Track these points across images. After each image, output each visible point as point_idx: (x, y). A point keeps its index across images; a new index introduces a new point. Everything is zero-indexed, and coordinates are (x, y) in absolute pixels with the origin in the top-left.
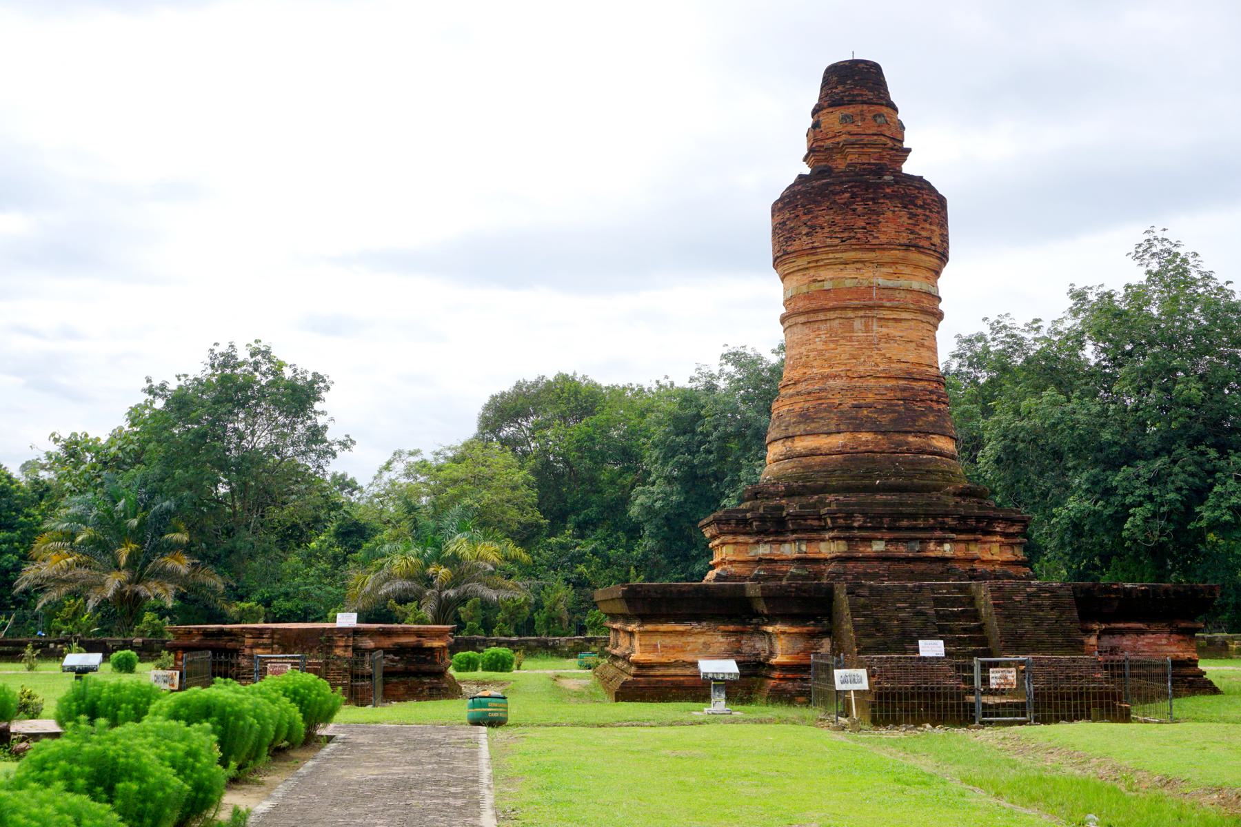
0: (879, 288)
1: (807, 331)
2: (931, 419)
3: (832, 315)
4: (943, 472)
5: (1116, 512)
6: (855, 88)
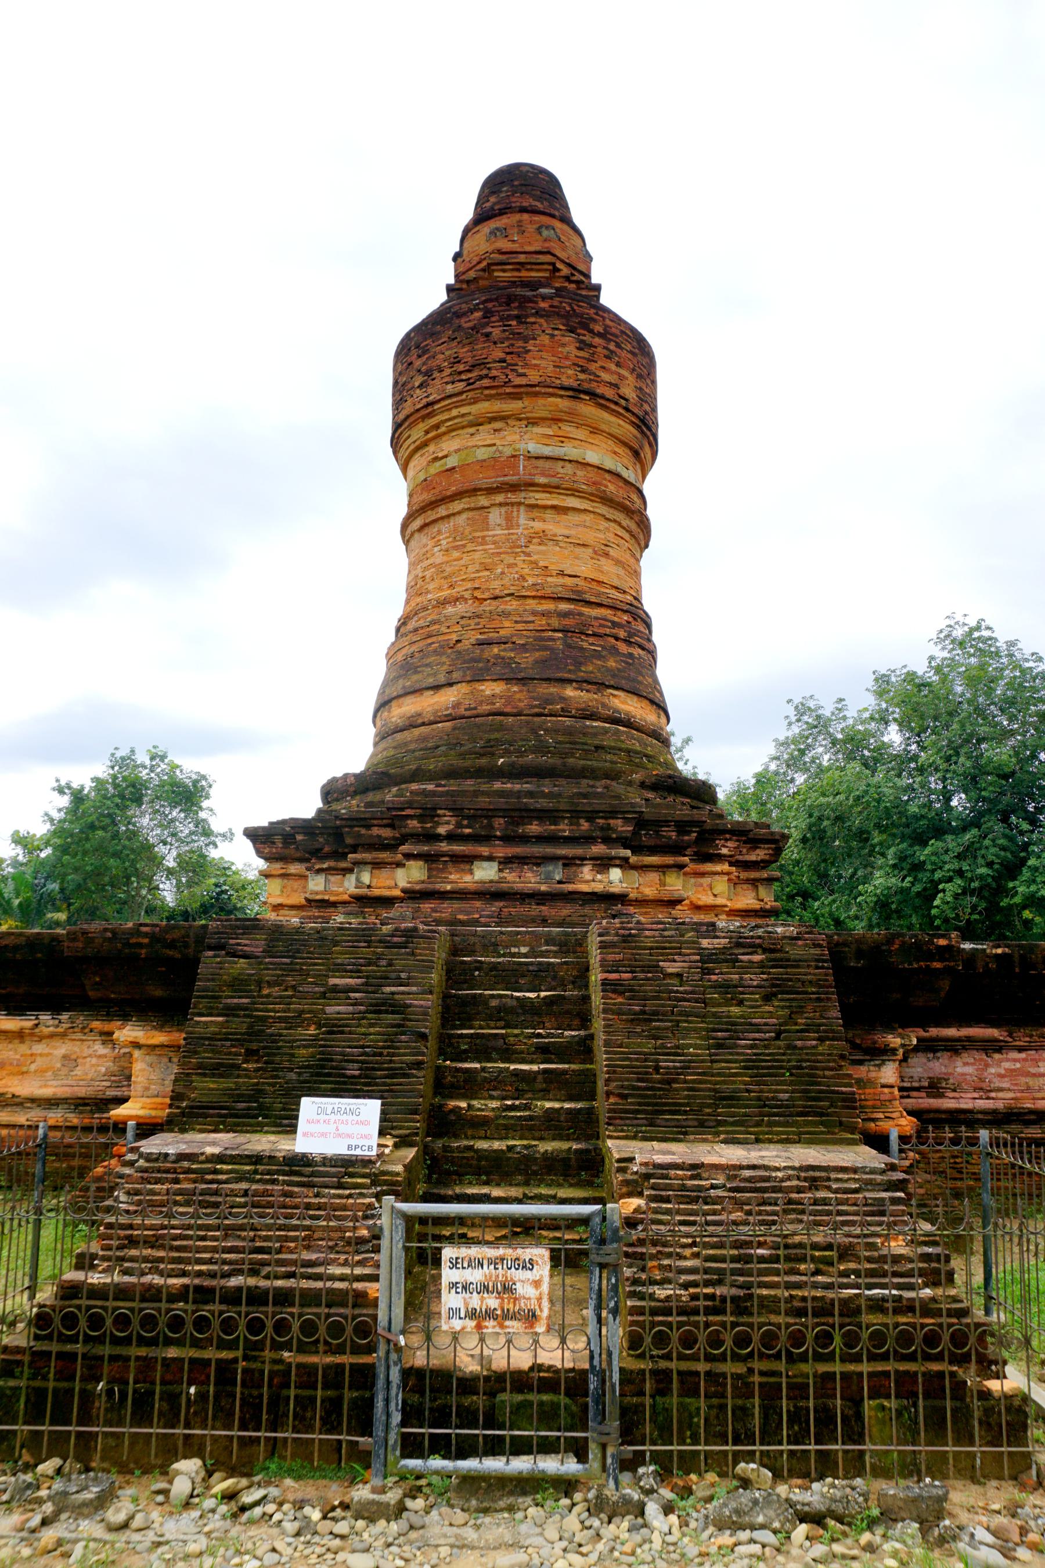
0: (530, 457)
1: (424, 540)
2: (612, 663)
3: (457, 506)
4: (628, 751)
5: (925, 889)
6: (522, 196)
